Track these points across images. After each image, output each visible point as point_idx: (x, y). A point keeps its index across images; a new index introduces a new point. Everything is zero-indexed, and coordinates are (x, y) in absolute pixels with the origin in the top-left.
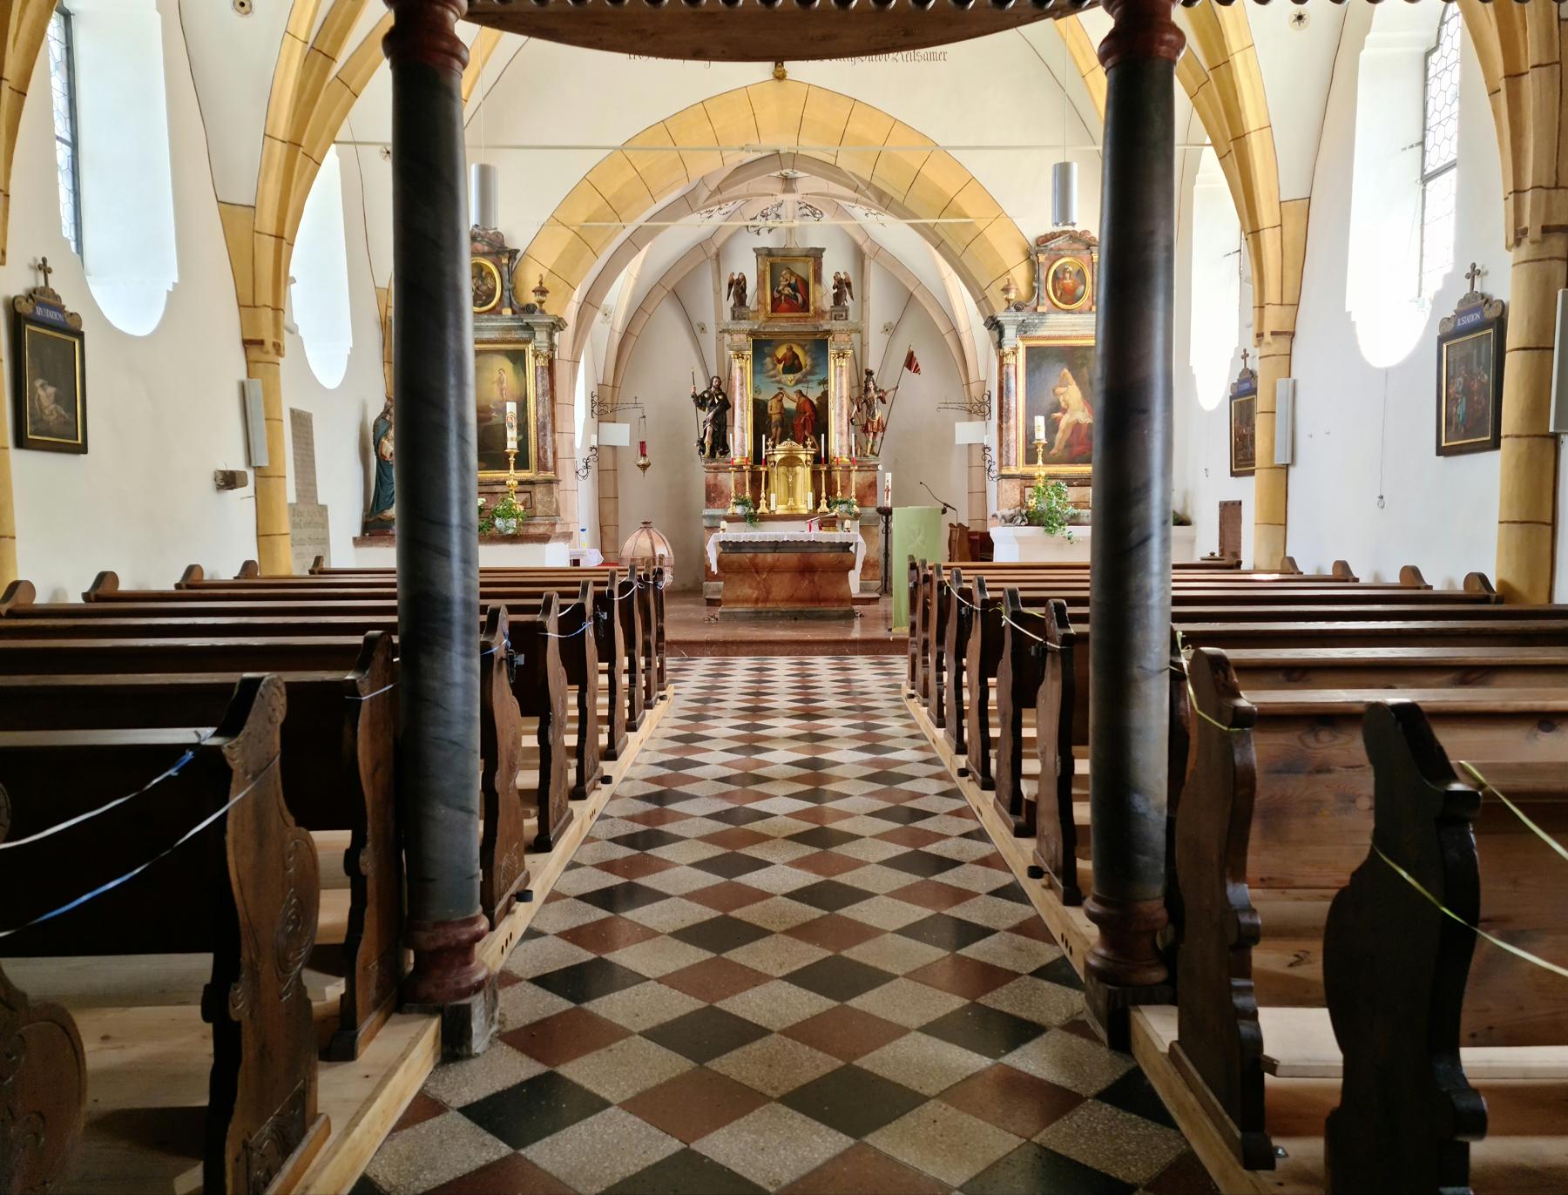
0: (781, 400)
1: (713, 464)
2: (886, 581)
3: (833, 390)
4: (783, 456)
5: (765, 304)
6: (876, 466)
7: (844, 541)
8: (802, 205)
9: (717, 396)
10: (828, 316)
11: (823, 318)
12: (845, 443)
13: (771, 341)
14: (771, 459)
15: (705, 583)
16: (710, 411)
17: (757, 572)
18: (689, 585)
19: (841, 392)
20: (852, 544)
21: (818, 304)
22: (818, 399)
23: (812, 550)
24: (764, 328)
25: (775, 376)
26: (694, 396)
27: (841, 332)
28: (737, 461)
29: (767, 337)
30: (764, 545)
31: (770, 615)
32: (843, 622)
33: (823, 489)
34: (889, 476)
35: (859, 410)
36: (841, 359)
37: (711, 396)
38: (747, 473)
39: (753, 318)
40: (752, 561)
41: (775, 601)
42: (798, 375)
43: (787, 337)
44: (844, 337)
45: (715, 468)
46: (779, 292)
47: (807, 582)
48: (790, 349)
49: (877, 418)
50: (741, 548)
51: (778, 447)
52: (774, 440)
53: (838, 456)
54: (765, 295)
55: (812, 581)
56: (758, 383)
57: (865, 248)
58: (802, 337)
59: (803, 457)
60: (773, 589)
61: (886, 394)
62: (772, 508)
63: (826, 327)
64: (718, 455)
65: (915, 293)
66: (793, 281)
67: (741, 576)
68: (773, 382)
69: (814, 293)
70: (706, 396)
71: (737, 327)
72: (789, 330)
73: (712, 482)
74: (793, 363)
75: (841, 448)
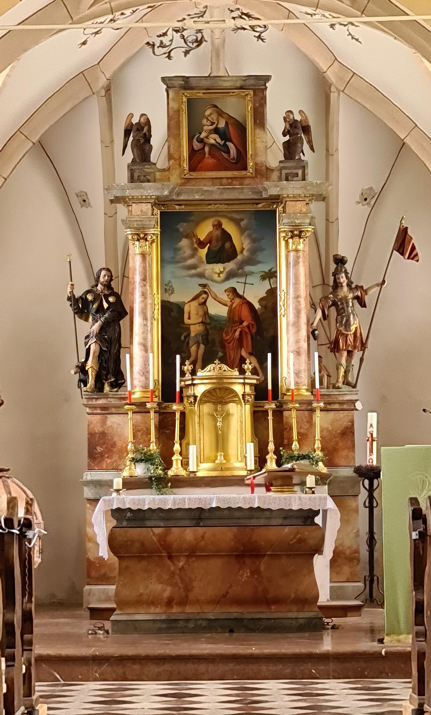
0: (204, 303)
1: (101, 402)
2: (372, 582)
3: (284, 287)
4: (208, 387)
5: (179, 159)
6: (353, 402)
7: (306, 507)
8: (235, 14)
9: (106, 297)
10: (275, 175)
11: (268, 179)
12: (303, 366)
13: (189, 213)
14: (190, 392)
15: (87, 587)
16: (95, 321)
17: (170, 557)
18: (61, 595)
19: (296, 289)
20: (317, 513)
21: (259, 159)
22: (261, 301)
23: (254, 522)
24: (178, 194)
25: (194, 267)
26: (72, 298)
27: (296, 199)
28: (137, 395)
29: (183, 208)
30: (180, 514)
31: (191, 625)
32: (307, 635)
33: (271, 438)
34: (373, 418)
35: (325, 317)
36: (296, 239)
37: (97, 297)
38: (152, 414)
39: (161, 180)
40: (162, 538)
41: (197, 602)
42: (231, 265)
43: (212, 208)
44: (300, 206)
45: (104, 408)
46: (201, 141)
47: (247, 573)
48: (218, 225)
49: (353, 328)
50: (143, 519)
51: (200, 374)
52: (194, 363)
53: (292, 387)
54: (180, 146)
55: (256, 572)
56: (168, 278)
57: (331, 75)
58: (231, 208)
59: (238, 389)
60: (196, 584)
61: (366, 292)
62: (192, 467)
63: (273, 191)
64: (107, 388)
65: (407, 141)
66: (222, 125)
67: (144, 563)
68: (193, 276)
69: (254, 142)
70: (90, 297)
71: (136, 193)
72: (217, 197)
73: (98, 429)
74: (223, 246)
75: (297, 374)
